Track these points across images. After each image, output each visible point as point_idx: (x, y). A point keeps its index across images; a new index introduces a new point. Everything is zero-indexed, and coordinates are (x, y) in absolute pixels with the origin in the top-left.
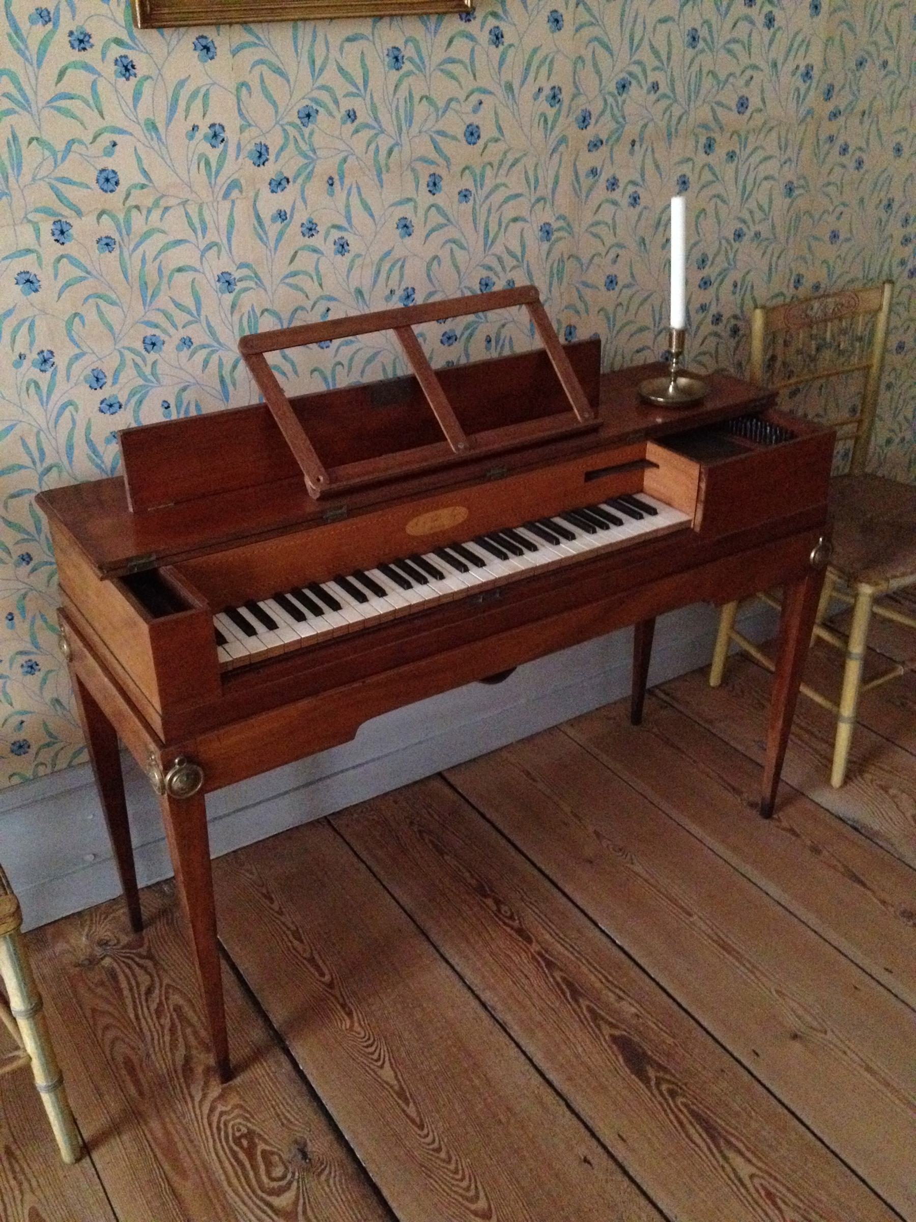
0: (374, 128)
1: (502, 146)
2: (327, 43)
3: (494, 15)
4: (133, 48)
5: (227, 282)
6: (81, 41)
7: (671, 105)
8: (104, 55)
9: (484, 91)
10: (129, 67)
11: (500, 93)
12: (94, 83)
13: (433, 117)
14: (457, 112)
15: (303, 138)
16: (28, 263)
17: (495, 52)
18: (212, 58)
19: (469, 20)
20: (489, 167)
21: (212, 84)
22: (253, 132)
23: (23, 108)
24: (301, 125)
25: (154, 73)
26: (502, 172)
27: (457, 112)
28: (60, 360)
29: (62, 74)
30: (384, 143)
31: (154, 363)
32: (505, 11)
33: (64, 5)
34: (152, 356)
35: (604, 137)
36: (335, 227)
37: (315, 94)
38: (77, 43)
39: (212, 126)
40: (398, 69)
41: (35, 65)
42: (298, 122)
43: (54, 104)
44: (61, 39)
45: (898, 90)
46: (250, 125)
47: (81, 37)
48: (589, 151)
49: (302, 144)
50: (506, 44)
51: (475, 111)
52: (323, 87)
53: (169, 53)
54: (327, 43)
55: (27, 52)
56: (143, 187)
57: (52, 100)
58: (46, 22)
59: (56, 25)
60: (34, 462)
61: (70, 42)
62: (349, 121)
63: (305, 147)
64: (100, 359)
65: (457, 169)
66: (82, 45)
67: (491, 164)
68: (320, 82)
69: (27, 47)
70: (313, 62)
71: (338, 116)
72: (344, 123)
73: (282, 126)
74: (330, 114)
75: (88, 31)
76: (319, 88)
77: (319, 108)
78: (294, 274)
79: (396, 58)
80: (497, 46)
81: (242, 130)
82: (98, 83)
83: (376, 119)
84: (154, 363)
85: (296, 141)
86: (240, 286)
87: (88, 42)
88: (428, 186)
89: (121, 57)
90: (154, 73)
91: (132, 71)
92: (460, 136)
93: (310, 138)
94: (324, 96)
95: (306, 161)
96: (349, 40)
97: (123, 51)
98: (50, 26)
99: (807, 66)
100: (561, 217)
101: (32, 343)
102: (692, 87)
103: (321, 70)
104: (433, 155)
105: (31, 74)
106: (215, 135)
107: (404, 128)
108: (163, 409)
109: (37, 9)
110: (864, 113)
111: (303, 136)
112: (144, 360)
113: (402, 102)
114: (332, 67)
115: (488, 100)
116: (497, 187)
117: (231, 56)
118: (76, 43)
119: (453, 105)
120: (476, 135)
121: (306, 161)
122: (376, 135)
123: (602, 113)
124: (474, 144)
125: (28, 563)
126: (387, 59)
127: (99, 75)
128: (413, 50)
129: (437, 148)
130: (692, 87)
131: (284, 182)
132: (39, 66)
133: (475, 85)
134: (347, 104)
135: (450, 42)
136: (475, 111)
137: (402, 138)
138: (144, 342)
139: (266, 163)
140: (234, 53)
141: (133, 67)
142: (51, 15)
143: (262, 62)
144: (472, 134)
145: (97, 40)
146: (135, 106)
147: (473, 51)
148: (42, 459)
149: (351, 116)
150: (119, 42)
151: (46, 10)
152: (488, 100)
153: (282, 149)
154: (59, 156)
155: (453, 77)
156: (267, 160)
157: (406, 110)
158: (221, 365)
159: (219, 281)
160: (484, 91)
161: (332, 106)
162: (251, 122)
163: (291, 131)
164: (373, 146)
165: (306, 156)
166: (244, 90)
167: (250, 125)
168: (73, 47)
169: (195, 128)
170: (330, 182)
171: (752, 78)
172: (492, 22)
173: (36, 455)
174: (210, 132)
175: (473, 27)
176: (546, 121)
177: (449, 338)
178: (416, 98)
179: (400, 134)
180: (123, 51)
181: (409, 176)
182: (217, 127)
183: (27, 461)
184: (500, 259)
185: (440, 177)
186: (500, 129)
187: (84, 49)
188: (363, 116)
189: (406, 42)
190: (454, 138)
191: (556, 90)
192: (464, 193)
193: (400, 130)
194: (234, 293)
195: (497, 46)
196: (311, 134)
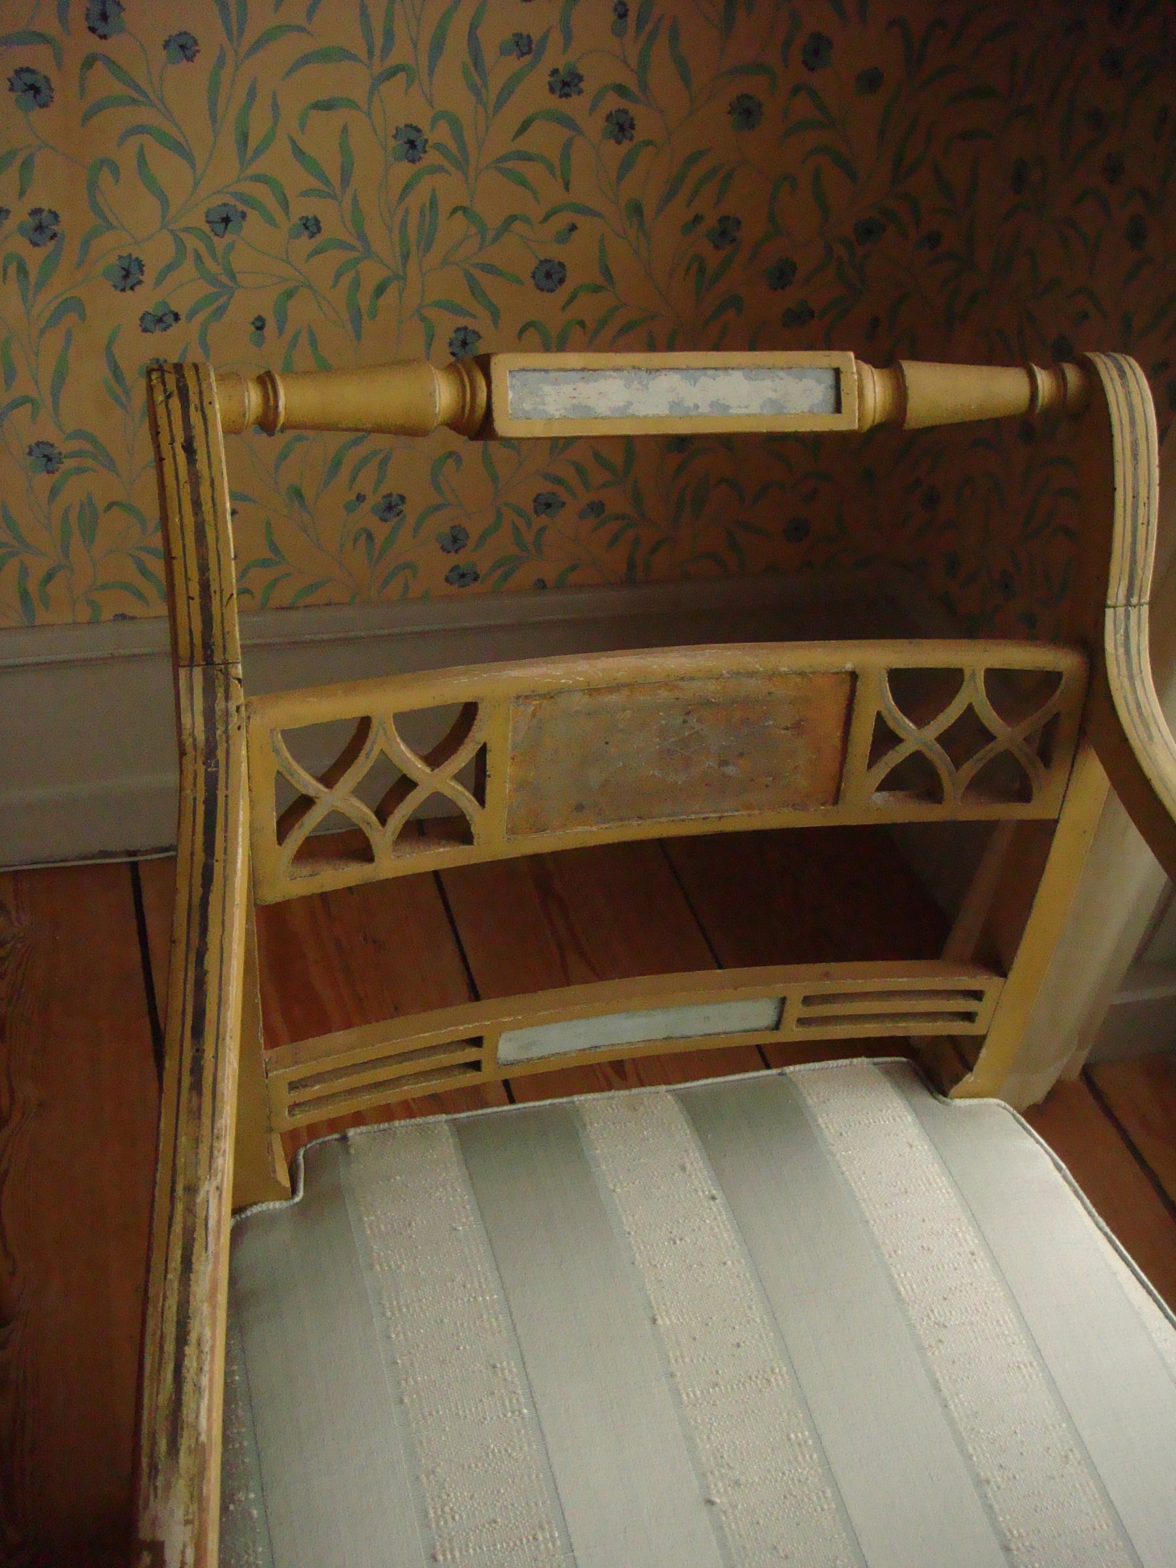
0: (352, 248)
5: (46, 457)
7: (357, 261)
8: (593, 107)
10: (626, 126)
16: (39, 58)
18: (44, 106)
19: (567, 95)
24: (211, 235)
28: (411, 512)
29: (525, 126)
30: (372, 274)
31: (542, 530)
34: (543, 520)
35: (181, 307)
37: (247, 188)
38: (560, 85)
39: (36, 212)
40: (413, 161)
41: (490, 111)
42: (207, 228)
44: (539, 79)
45: (369, 285)
48: (145, 330)
49: (208, 261)
52: (259, 179)
55: (484, 91)
57: (504, 159)
58: (523, 54)
60: (370, 53)
66: (566, 90)
67: (582, 324)
70: (244, 138)
73: (172, 232)
74: (272, 221)
79: (412, 144)
83: (362, 236)
84: (542, 530)
85: (198, 257)
86: (69, 463)
87: (576, 85)
94: (261, 192)
95: (213, 290)
97: (622, 103)
98: (527, 59)
99: (723, 220)
100: (79, 434)
101: (379, 482)
102: (413, 234)
103: (258, 152)
106: (40, 228)
108: (614, 17)
110: (260, 324)
111: (211, 249)
112: (529, 524)
113: (413, 220)
119: (517, 226)
120: (556, 278)
121: (213, 290)
122: (357, 261)
123: (171, 267)
125: (312, 235)
126: (392, 143)
130: (413, 234)
131: (169, 319)
134: (301, 208)
138: (535, 501)
139: (137, 288)
143: (140, 130)
145: (589, 86)
147: (568, 146)
148: (386, 51)
149: (311, 226)
150: (621, 90)
151: (529, 36)
155: (523, 183)
156: (140, 282)
158: (24, 573)
159: (30, 453)
161: (278, 213)
162: (112, 219)
163: (192, 242)
164: (346, 280)
165: (214, 281)
166: (105, 175)
170: (259, 324)
171: (573, 228)
173: (379, 41)
174: (31, 222)
176: (702, 270)
177: (463, 576)
178: (445, 207)
179: (404, 264)
180: (622, 103)
182: (45, 214)
183: (362, 54)
184: (580, 470)
188: (333, 227)
189: (434, 121)
193: (406, 257)
194: (57, 475)
196: (231, 247)
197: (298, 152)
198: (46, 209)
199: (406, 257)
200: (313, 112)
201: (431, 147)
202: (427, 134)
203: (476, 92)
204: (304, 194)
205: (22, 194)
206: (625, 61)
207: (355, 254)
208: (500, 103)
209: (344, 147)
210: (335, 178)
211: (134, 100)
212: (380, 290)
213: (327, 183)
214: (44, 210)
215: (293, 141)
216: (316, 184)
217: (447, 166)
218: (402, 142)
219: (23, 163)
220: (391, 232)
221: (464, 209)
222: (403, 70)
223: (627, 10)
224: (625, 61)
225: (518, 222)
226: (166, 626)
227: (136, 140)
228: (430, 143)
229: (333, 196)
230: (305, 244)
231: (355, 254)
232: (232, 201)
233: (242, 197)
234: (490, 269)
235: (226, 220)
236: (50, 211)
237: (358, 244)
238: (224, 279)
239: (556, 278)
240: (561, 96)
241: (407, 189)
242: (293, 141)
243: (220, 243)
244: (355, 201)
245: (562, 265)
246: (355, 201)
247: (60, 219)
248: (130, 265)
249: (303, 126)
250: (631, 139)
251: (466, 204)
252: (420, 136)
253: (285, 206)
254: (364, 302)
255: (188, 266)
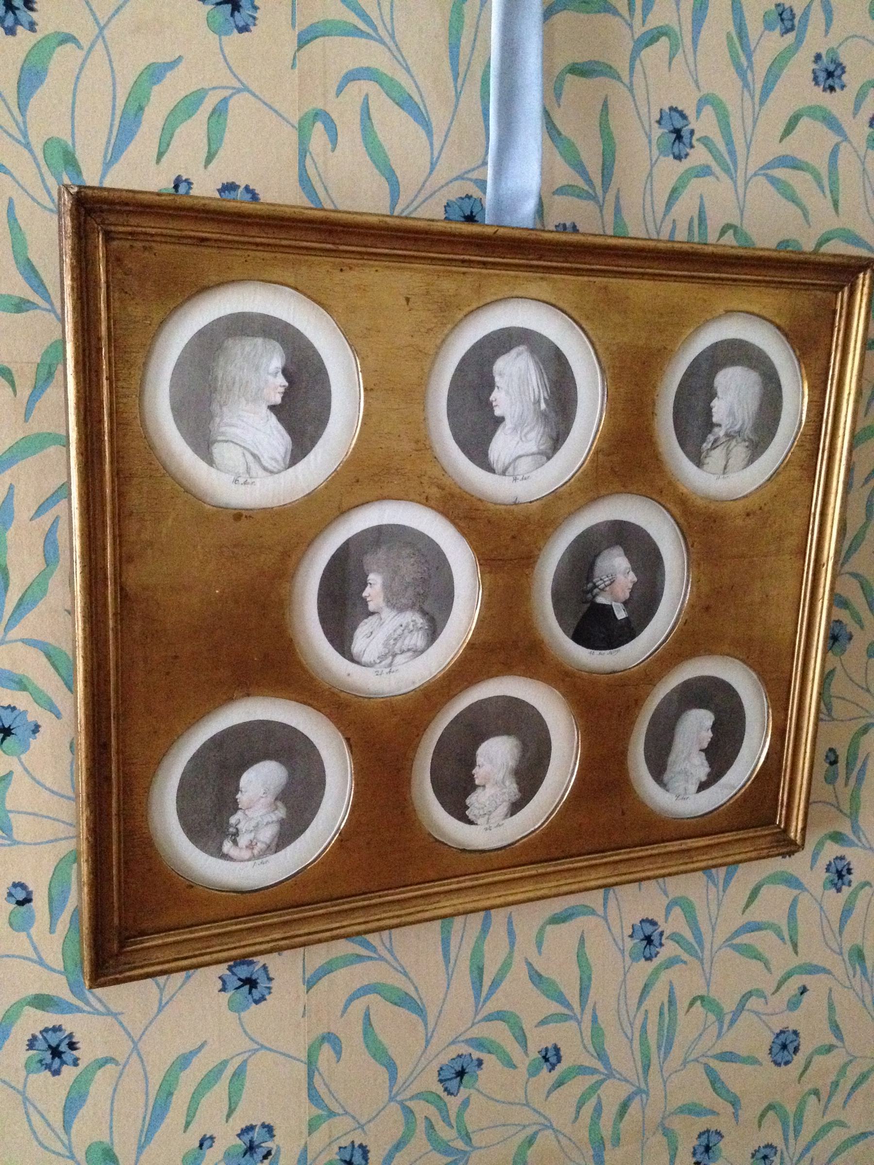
1: (834, 1061)
2: (511, 933)
3: (837, 837)
4: (79, 1010)
6: (830, 75)
9: (812, 969)
10: (63, 1047)
11: (839, 967)
12: (834, 153)
13: (714, 1029)
14: (757, 1013)
15: (446, 1119)
17: (835, 901)
20: (813, 1097)
21: (239, 91)
22: (341, 1125)
23: (727, 170)
24: (444, 1095)
25: (122, 1049)
26: (838, 1098)
27: (757, 1013)
32: (855, 829)
33: (817, 6)
36: (42, 1002)
43: (737, 941)
46: (332, 1114)
47: (831, 68)
50: (854, 885)
51: (793, 1005)
53: (161, 1008)
54: (511, 933)
55: (749, 75)
56: (830, 1049)
58: (787, 31)
59: (799, 41)
61: (814, 71)
62: (545, 1067)
63: (446, 1133)
64: (362, 1127)
65: (750, 1111)
66: (830, 82)
67: (816, 1092)
68: (491, 1006)
69: (751, 66)
71: (523, 1062)
72: (533, 1072)
73: (401, 1103)
74: (510, 1064)
75: (844, 59)
76: (489, 1018)
77: (484, 1056)
78: (755, 927)
80: (839, 890)
81: (313, 1126)
82: (841, 148)
83: (602, 1056)
85: (431, 1126)
87: (840, 77)
88: (694, 1154)
89: (46, 1030)
90: (122, 1049)
91: (68, 1055)
92: (763, 1055)
93: (459, 1115)
94: (499, 1033)
96: (557, 920)
98: (791, 37)
103: (495, 984)
104: (707, 1097)
105: (748, 114)
107: (655, 1061)
109: (778, 5)
113: (653, 1017)
114: (519, 972)
115: (816, 983)
116: (824, 1130)
117: (304, 988)
118: (822, 76)
119: (754, 1003)
122: (600, 1083)
124: (787, 1063)
125: (553, 1067)
126: (629, 943)
127: (846, 139)
128: (682, 919)
129: (715, 1081)
132: (762, 103)
133: (795, 961)
134: (539, 1039)
135: (754, 894)
136: (793, 1005)
137: (651, 1078)
140: (310, 984)
141: (72, 1046)
142: (796, 21)
144: (784, 1047)
146: (67, 1126)
147: (834, 153)
152: (816, 983)
153: (398, 1146)
154: (727, 1019)
157: (660, 1029)
160: (812, 969)
163: (422, 1109)
166: (318, 134)
167: (332, 1114)
168: (816, 79)
169: (205, 1142)
171: (804, 990)
172: (831, 850)
174: (241, 1144)
175: (796, 864)
178: (682, 1003)
181: (657, 1141)
185: (718, 1133)
186: (836, 1029)
187: (832, 89)
189: (668, 909)
190: (753, 1061)
191: (256, 1135)
192: (764, 1152)
193: (646, 1068)
195: (839, 890)
196: (466, 1103)
197: (536, 978)
198: (259, 1124)
199: (646, 1068)
200: (569, 77)
201: (698, 140)
202: (662, 926)
203: (742, 73)
204: (543, 1022)
205: (210, 158)
206: (41, 962)
207: (596, 1077)
208: (766, 92)
209: (581, 956)
210: (573, 995)
211: (358, 956)
212: (624, 1107)
213: (589, 181)
214: (238, 187)
215: (529, 964)
216: (555, 1008)
217: (685, 956)
218: (666, 131)
219: (234, 1075)
220: (631, 1041)
221: (702, 998)
222: (665, 34)
223: (837, 757)
224: (41, 962)
225: (754, 997)
226: (393, 931)
227: (367, 86)
228: (696, 136)
229: (594, 198)
230: (547, 1077)
231: (596, 1077)
232: (465, 1049)
233: (479, 1044)
234: (727, 1057)
235: (461, 1074)
236: (264, 1126)
237: (599, 1066)
238: (460, 1145)
239: (791, 1048)
240: (824, 90)
241: (674, 194)
242: (529, 964)
243: (453, 1103)
244: (595, 1019)
245: (795, 1033)
246: (595, 1019)
247: (275, 1133)
248: (352, 1156)
249: (539, 944)
250: (850, 885)
251: (702, 992)
252: (687, 125)
253: (522, 1039)
254: (606, 1131)
255: (419, 1142)
